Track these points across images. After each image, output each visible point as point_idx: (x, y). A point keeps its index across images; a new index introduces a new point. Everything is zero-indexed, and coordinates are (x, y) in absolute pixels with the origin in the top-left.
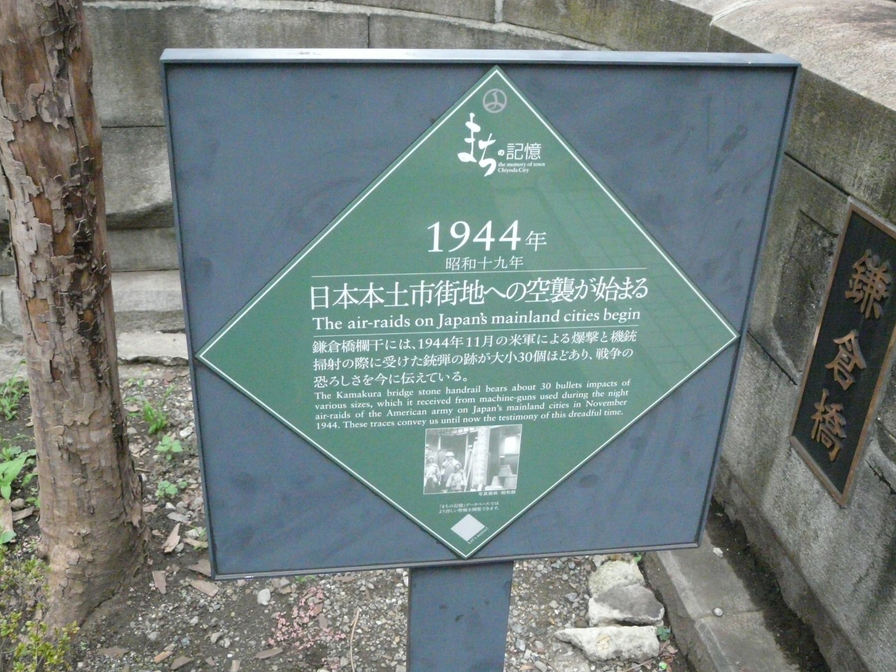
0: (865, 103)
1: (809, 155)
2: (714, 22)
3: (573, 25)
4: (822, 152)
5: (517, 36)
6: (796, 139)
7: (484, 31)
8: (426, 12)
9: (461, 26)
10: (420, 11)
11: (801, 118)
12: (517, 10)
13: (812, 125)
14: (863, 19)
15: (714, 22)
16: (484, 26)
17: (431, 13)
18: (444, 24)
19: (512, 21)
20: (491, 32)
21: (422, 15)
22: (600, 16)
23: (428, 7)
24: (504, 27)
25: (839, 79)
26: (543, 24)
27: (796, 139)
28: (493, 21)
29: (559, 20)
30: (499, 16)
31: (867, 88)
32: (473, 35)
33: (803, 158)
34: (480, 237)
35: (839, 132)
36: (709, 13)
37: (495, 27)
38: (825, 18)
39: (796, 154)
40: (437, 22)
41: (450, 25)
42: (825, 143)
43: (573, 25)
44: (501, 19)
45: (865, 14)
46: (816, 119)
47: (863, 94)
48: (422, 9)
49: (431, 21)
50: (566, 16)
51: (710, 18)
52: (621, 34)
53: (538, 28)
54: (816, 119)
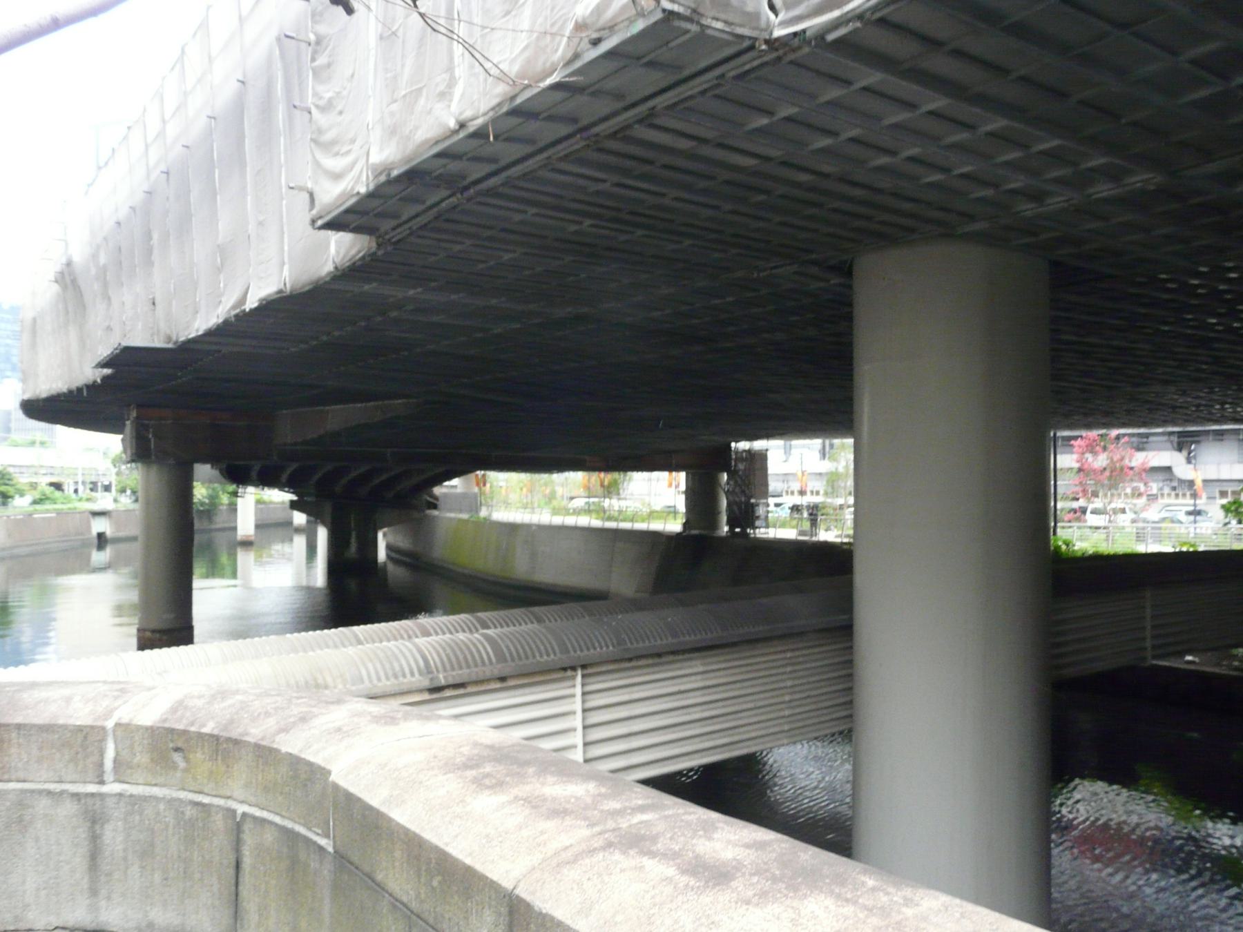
0: (469, 872)
1: (435, 918)
2: (333, 778)
3: (195, 779)
4: (447, 916)
5: (131, 796)
6: (422, 902)
7: (93, 795)
8: (18, 781)
9: (62, 792)
10: (10, 781)
11: (423, 880)
12: (131, 768)
13: (433, 888)
14: (466, 767)
15: (333, 778)
16: (92, 788)
17: (24, 781)
18: (40, 792)
19: (127, 779)
20: (102, 796)
21: (12, 785)
22: (223, 768)
23: (21, 775)
24: (116, 788)
25: (447, 844)
26: (161, 780)
27: (422, 902)
28: (102, 782)
29: (179, 774)
30: (109, 776)
31: (471, 854)
32: (79, 800)
33: (431, 921)
34: (687, 31)
35: (456, 897)
36: (328, 767)
37: (105, 789)
38: (433, 768)
39: (425, 916)
40: (33, 791)
41: (49, 793)
42: (447, 907)
43: (195, 779)
44: (112, 779)
45: (470, 759)
46: (435, 883)
47: (468, 861)
48: (13, 777)
49: (23, 791)
50: (186, 770)
51: (329, 772)
52: (247, 785)
53: (156, 785)
54: (435, 883)
